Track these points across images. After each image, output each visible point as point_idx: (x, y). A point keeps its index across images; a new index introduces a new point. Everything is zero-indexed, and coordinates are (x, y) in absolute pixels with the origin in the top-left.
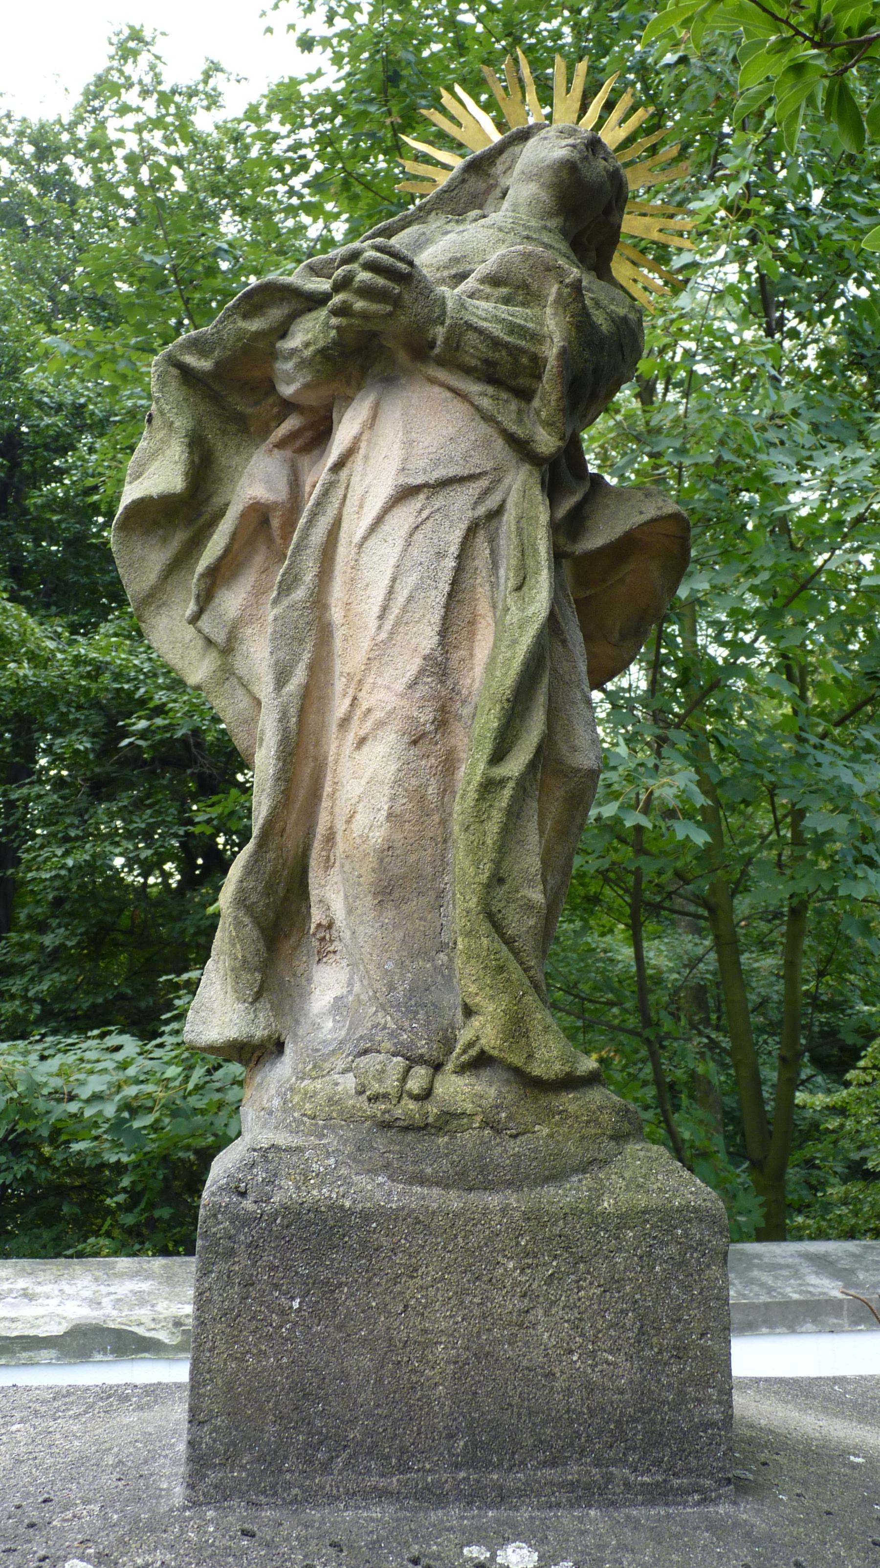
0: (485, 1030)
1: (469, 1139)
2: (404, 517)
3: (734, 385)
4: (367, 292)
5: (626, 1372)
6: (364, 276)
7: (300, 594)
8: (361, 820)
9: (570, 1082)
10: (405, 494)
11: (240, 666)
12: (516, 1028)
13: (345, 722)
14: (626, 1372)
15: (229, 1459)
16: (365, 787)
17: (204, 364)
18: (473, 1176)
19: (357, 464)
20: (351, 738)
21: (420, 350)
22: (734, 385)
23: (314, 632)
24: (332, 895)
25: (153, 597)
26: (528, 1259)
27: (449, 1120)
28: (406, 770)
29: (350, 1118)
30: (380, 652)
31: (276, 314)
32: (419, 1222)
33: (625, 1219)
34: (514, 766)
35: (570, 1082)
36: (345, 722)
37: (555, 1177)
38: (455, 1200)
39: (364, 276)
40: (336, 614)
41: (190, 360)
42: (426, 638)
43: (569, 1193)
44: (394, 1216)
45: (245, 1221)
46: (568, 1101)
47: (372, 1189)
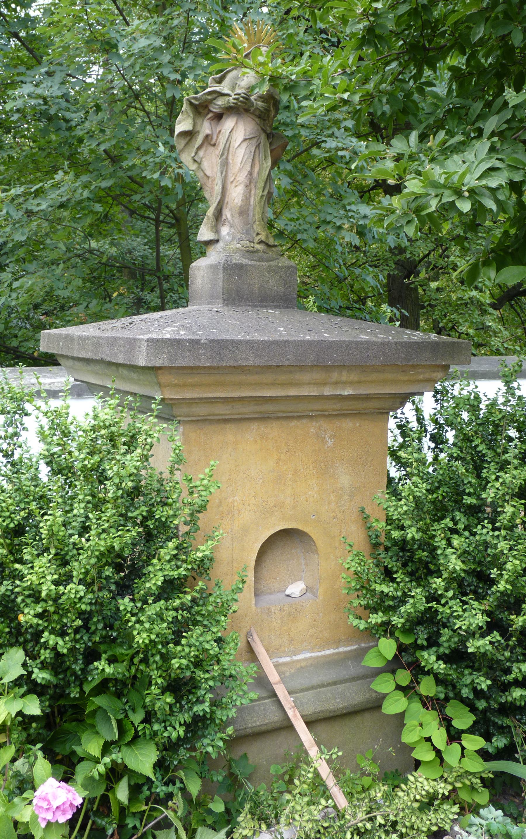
0: (262, 237)
1: (260, 254)
2: (245, 145)
3: (404, 555)
4: (241, 102)
5: (282, 290)
6: (241, 99)
7: (224, 157)
8: (236, 201)
9: (274, 246)
10: (245, 140)
11: (202, 167)
12: (267, 237)
13: (232, 182)
14: (282, 290)
15: (228, 300)
16: (236, 194)
17: (196, 103)
18: (261, 260)
19: (234, 132)
20: (234, 185)
21: (247, 111)
22: (404, 555)
23: (225, 164)
24: (227, 214)
25: (182, 151)
26: (269, 272)
27: (257, 251)
28: (245, 192)
29: (241, 250)
30: (240, 170)
31: (214, 96)
32: (254, 266)
33: (282, 267)
34: (265, 193)
35: (274, 246)
36: (232, 182)
37: (272, 261)
38: (258, 263)
39: (241, 99)
40: (230, 161)
41: (193, 101)
42: (249, 169)
43: (274, 263)
44: (250, 265)
45: (229, 265)
46: (273, 249)
47: (245, 261)
